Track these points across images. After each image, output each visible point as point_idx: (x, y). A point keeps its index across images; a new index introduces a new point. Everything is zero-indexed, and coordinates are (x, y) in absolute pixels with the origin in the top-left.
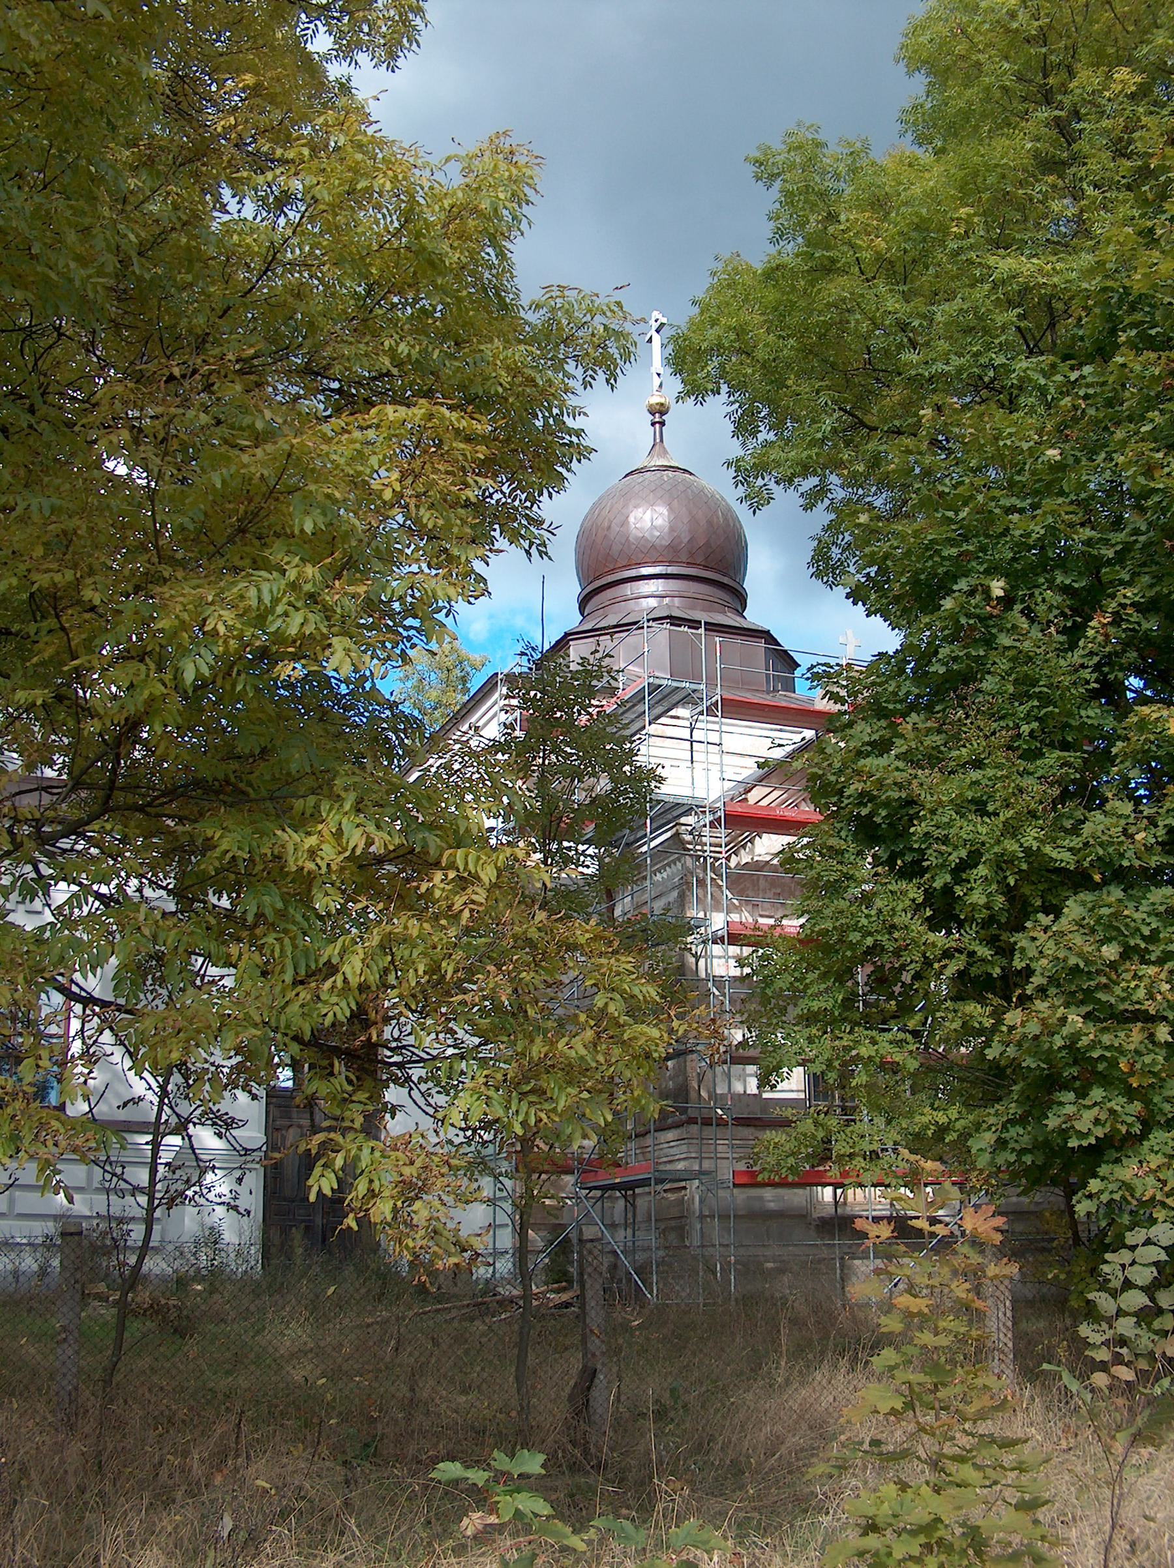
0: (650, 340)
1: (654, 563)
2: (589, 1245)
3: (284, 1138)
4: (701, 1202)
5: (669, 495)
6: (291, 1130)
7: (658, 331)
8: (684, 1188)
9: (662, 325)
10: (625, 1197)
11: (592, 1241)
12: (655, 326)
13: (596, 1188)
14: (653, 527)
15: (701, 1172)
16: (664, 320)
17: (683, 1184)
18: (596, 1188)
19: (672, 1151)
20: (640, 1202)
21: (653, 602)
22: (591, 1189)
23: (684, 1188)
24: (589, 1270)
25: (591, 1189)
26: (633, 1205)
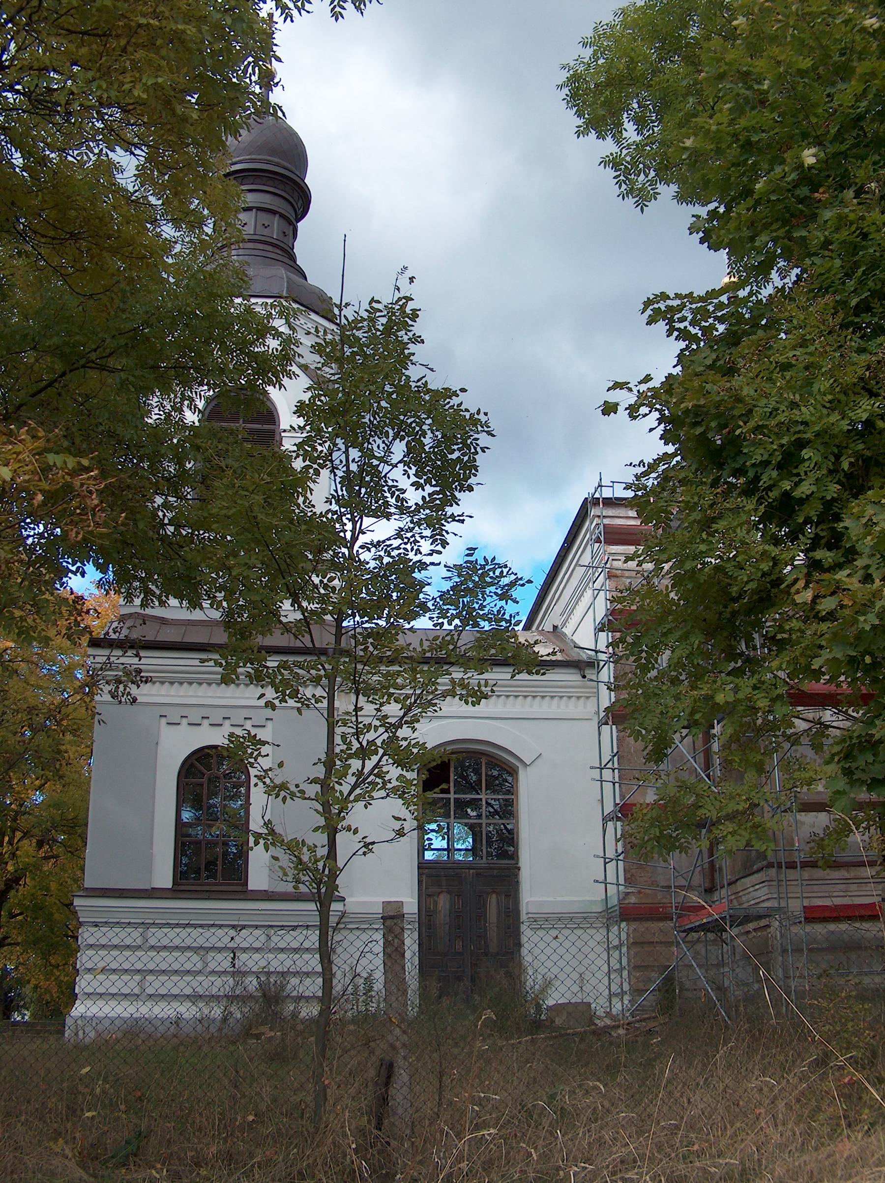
3: (436, 903)
6: (442, 896)
17: (763, 923)
19: (758, 894)
23: (768, 926)
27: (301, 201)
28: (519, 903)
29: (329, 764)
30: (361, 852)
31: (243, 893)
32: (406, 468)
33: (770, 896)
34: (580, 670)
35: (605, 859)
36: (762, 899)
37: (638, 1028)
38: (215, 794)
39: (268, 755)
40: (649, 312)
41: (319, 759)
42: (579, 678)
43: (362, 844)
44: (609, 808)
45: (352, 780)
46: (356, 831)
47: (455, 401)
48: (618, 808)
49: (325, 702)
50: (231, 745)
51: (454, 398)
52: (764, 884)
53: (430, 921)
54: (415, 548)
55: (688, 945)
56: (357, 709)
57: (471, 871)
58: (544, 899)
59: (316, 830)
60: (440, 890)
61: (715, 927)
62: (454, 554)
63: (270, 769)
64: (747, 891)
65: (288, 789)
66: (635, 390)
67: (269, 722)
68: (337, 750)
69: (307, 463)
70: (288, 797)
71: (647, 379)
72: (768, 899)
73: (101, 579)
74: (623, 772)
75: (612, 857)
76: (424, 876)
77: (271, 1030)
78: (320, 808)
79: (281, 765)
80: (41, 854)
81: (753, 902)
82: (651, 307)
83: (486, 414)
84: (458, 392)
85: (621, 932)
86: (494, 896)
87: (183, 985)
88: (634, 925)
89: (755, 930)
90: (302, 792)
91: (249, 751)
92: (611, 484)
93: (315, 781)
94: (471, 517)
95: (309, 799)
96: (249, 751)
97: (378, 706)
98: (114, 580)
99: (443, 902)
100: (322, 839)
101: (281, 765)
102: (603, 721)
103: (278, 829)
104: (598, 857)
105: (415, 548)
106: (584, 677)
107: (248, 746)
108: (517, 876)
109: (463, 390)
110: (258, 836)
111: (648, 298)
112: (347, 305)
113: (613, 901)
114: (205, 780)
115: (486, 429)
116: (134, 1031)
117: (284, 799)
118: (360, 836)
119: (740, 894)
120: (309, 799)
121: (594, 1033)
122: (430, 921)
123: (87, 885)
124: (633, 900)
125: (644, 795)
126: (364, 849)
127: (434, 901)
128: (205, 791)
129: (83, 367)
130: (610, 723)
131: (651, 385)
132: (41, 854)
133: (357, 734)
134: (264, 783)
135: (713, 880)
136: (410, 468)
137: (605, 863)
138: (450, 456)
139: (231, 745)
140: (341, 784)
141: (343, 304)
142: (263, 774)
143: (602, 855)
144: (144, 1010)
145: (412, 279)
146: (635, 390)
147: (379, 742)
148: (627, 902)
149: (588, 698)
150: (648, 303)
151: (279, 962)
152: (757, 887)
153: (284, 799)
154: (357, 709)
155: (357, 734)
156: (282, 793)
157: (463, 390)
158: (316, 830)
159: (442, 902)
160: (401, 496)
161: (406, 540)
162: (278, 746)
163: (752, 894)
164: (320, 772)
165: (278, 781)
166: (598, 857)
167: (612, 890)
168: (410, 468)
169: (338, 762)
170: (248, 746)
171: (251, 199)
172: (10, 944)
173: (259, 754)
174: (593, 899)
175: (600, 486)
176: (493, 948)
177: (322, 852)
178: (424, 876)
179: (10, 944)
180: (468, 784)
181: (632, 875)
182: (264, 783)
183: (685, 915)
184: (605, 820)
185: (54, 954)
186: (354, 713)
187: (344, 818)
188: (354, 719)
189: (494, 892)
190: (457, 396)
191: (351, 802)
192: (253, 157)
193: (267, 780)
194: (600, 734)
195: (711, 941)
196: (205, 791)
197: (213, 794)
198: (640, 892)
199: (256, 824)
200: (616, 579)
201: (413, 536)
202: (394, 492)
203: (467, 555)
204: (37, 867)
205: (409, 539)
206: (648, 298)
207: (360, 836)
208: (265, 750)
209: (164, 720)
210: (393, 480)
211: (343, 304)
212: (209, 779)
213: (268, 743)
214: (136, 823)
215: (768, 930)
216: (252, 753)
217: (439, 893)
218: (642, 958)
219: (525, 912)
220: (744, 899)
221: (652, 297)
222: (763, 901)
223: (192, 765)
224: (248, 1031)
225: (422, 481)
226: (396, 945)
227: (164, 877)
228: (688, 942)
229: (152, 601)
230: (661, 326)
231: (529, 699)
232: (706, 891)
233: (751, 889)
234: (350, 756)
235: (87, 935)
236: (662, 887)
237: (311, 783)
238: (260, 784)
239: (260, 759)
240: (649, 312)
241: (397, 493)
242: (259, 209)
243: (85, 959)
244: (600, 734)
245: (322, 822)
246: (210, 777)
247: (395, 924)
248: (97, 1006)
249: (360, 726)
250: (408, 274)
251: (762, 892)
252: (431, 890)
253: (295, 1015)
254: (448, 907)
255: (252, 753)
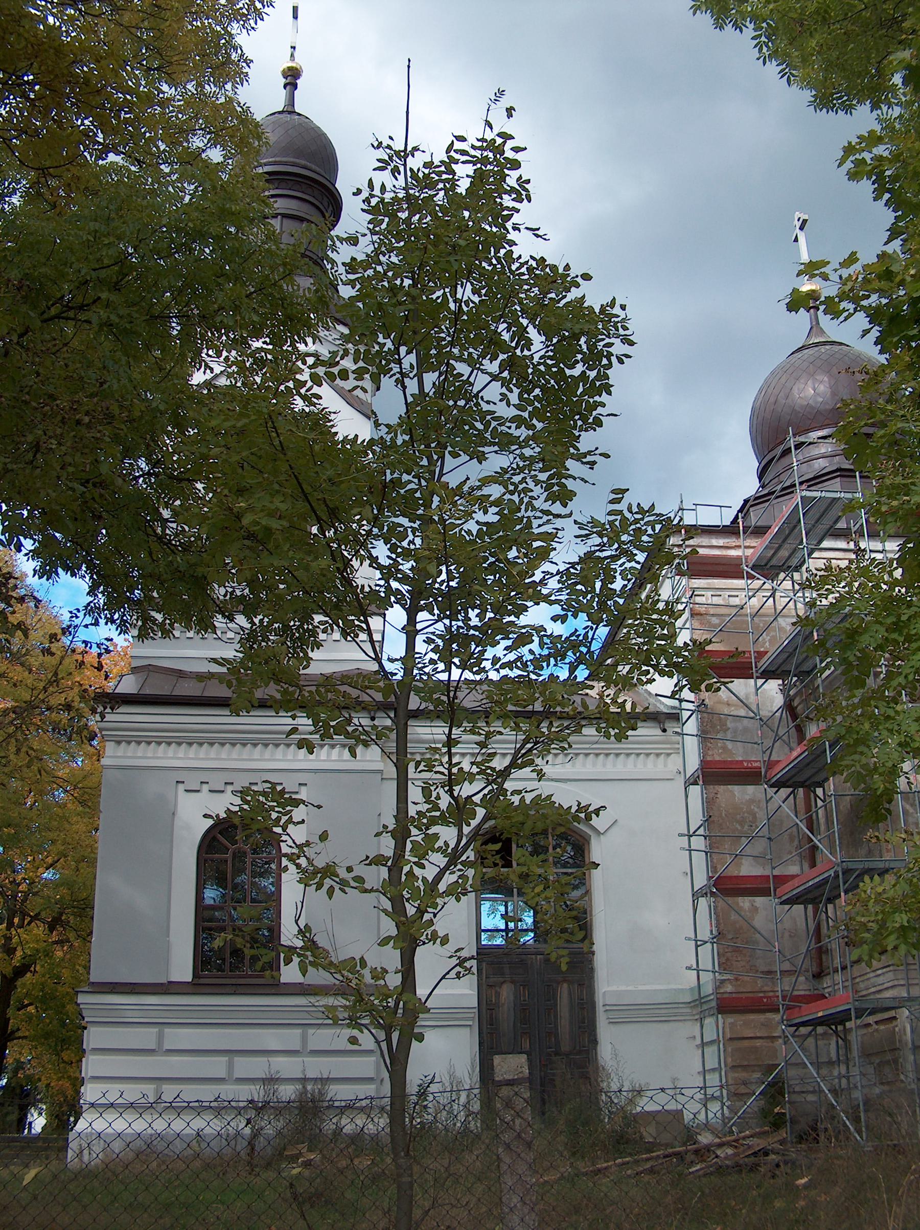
0: (796, 240)
1: (821, 428)
2: (505, 1091)
3: (498, 995)
4: (912, 1031)
5: (826, 366)
6: (505, 986)
7: (801, 228)
8: (895, 1018)
9: (805, 221)
10: (836, 1032)
11: (510, 1083)
12: (798, 224)
13: (804, 1024)
14: (816, 394)
15: (910, 999)
16: (806, 217)
17: (892, 1013)
18: (804, 1024)
19: (880, 980)
20: (852, 1037)
21: (822, 463)
22: (798, 1025)
23: (895, 1018)
24: (506, 1137)
25: (798, 1025)
26: (845, 1040)
27: (331, 208)
28: (594, 993)
29: (400, 835)
30: (453, 974)
31: (277, 988)
32: (504, 390)
33: (896, 983)
34: (660, 723)
35: (696, 941)
36: (886, 986)
37: (749, 1147)
38: (243, 871)
39: (303, 822)
40: (848, 165)
41: (385, 827)
42: (658, 732)
43: (454, 961)
44: (701, 880)
45: (439, 860)
46: (445, 940)
47: (574, 294)
48: (712, 882)
49: (393, 736)
50: (246, 807)
51: (573, 289)
52: (888, 969)
53: (491, 1015)
54: (526, 500)
55: (796, 1039)
56: (450, 742)
57: (539, 957)
58: (623, 988)
59: (384, 942)
60: (502, 980)
61: (837, 1020)
62: (591, 503)
63: (308, 844)
64: (866, 977)
65: (337, 876)
66: (834, 277)
67: (303, 788)
68: (412, 811)
69: (361, 364)
70: (337, 887)
71: (852, 259)
72: (892, 987)
73: (89, 604)
74: (714, 839)
75: (707, 939)
76: (484, 964)
77: (310, 1150)
78: (387, 905)
79: (324, 837)
80: (55, 937)
81: (873, 990)
82: (852, 158)
83: (623, 307)
84: (579, 280)
85: (712, 1027)
86: (565, 985)
87: (206, 1093)
88: (730, 1019)
89: (876, 1023)
90: (360, 879)
91: (274, 815)
92: (694, 507)
93: (378, 860)
94: (607, 456)
95: (372, 890)
96: (274, 815)
97: (482, 738)
98: (105, 604)
99: (507, 993)
100: (391, 958)
101: (324, 837)
102: (692, 781)
103: (321, 941)
104: (689, 939)
105: (526, 500)
106: (664, 731)
107: (272, 808)
108: (591, 961)
109: (587, 277)
110: (292, 949)
111: (850, 143)
112: (416, 149)
113: (708, 989)
114: (229, 855)
115: (621, 332)
116: (146, 1151)
117: (330, 892)
118: (451, 947)
119: (857, 980)
120: (372, 890)
121: (696, 1152)
122: (491, 1015)
123: (93, 979)
124: (729, 988)
125: (739, 865)
126: (458, 969)
127: (496, 992)
128: (229, 870)
129: (58, 317)
130: (701, 783)
131: (857, 267)
132: (55, 937)
133: (451, 783)
134: (298, 866)
135: (820, 964)
136: (511, 391)
137: (697, 946)
138: (568, 372)
139: (246, 807)
140: (422, 867)
141: (409, 149)
142: (295, 851)
143: (693, 937)
144: (160, 1125)
145: (510, 111)
146: (834, 277)
147: (477, 799)
148: (722, 991)
149: (669, 755)
150: (849, 150)
151: (316, 1067)
152: (879, 972)
153: (330, 892)
154: (450, 742)
155: (451, 783)
156: (328, 882)
157: (587, 277)
158: (384, 942)
159: (505, 993)
160: (500, 429)
161: (511, 488)
162: (319, 807)
163: (872, 980)
164: (387, 846)
165: (320, 863)
166: (689, 939)
167: (707, 978)
168: (511, 391)
169: (414, 831)
170: (272, 808)
171: (281, 205)
172: (19, 1038)
173: (290, 821)
174: (680, 987)
175: (681, 509)
176: (565, 1047)
177: (394, 980)
178: (484, 964)
179: (19, 1038)
180: (536, 853)
181: (727, 959)
182: (298, 866)
183: (795, 1007)
184: (696, 896)
185: (67, 1049)
186: (445, 750)
187: (431, 923)
188: (445, 759)
189: (565, 981)
190: (578, 286)
191: (441, 895)
192: (278, 159)
193: (303, 861)
194: (687, 796)
195: (821, 1035)
196: (229, 870)
197: (240, 871)
198: (736, 979)
199: (289, 934)
200: (699, 617)
201: (524, 480)
202: (489, 423)
203: (612, 502)
204: (48, 954)
205: (516, 486)
206: (850, 143)
207: (451, 947)
208: (299, 813)
209: (181, 787)
210: (488, 402)
211: (409, 149)
212: (234, 854)
213: (303, 802)
214: (152, 909)
215: (894, 1023)
216: (278, 819)
217: (502, 983)
218: (741, 1058)
219: (601, 1004)
220: (862, 986)
221: (854, 141)
222: (887, 989)
223: (214, 838)
224: (280, 1154)
225: (526, 415)
226: (517, 1128)
227: (182, 968)
228: (798, 1036)
229: (153, 631)
230: (866, 186)
231: (602, 757)
232: (814, 976)
233: (872, 975)
234: (433, 822)
235: (93, 1037)
236: (762, 972)
237: (370, 864)
238: (292, 867)
239: (291, 829)
240: (848, 165)
241: (494, 424)
242: (285, 216)
243: (91, 1065)
244: (687, 796)
245: (389, 927)
246: (238, 851)
247: (516, 1094)
248: (101, 1127)
249: (455, 770)
250: (505, 102)
251: (886, 978)
252: (492, 980)
253: (339, 1131)
254: (512, 998)
255: (278, 819)
